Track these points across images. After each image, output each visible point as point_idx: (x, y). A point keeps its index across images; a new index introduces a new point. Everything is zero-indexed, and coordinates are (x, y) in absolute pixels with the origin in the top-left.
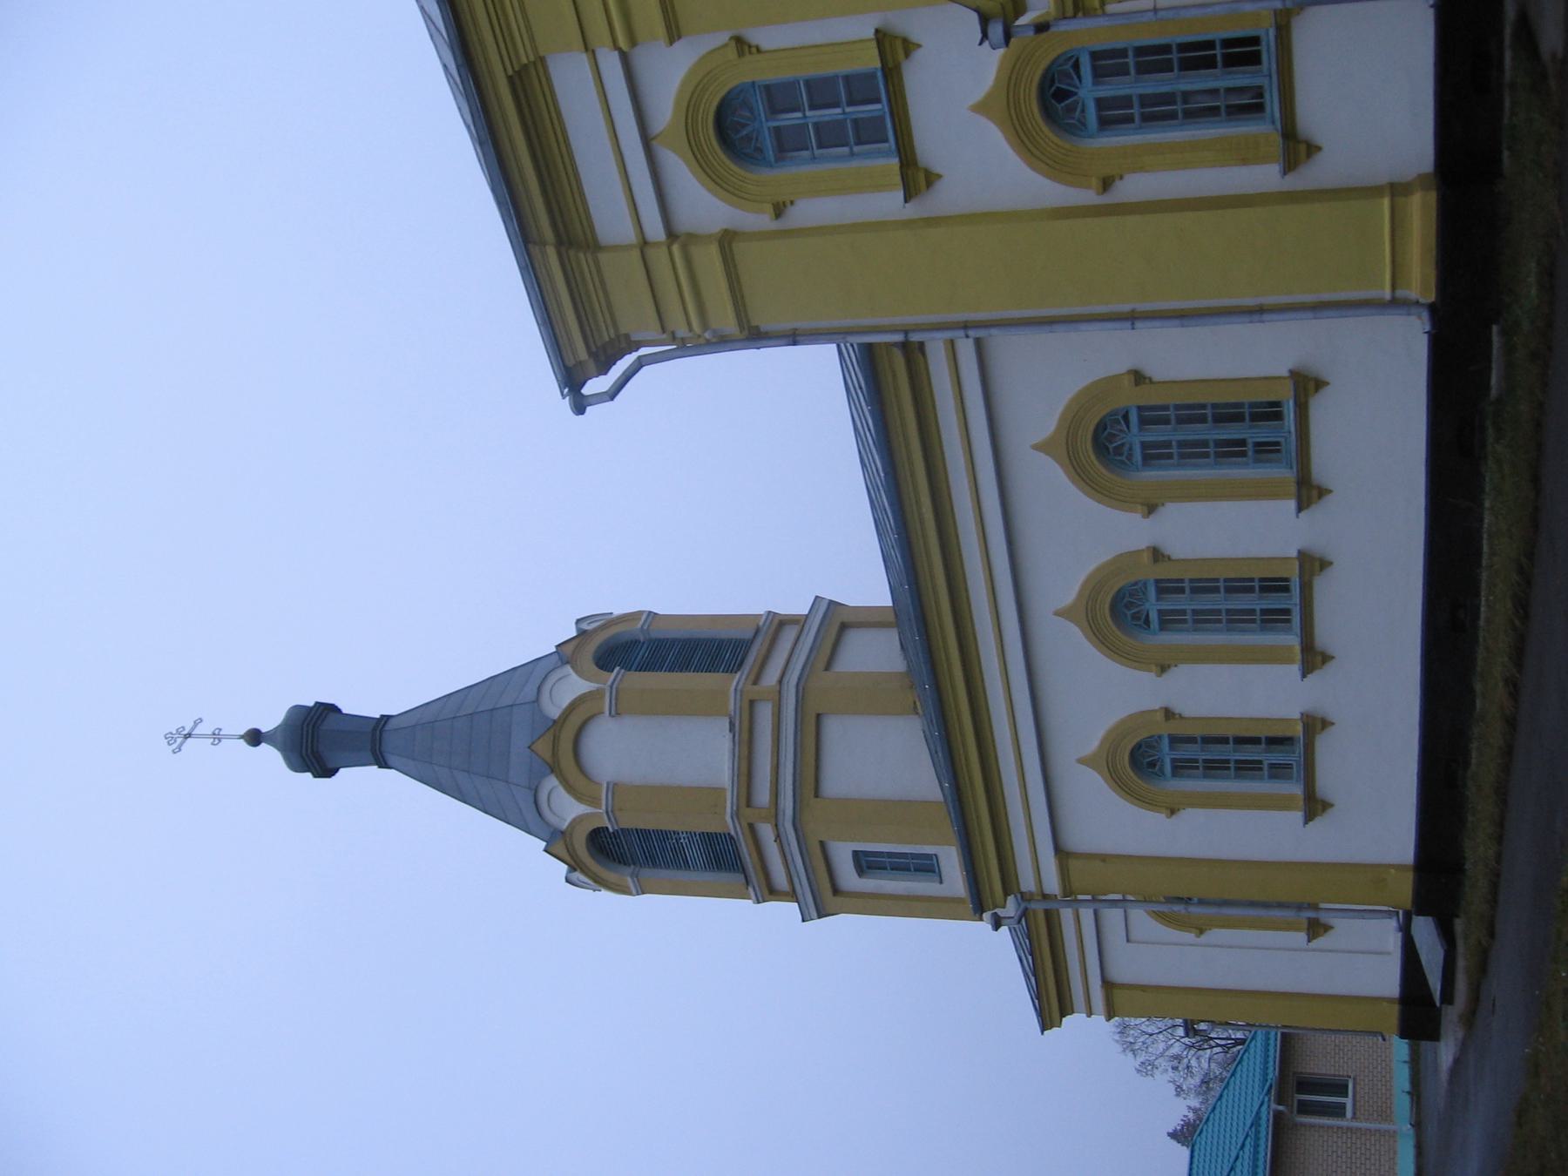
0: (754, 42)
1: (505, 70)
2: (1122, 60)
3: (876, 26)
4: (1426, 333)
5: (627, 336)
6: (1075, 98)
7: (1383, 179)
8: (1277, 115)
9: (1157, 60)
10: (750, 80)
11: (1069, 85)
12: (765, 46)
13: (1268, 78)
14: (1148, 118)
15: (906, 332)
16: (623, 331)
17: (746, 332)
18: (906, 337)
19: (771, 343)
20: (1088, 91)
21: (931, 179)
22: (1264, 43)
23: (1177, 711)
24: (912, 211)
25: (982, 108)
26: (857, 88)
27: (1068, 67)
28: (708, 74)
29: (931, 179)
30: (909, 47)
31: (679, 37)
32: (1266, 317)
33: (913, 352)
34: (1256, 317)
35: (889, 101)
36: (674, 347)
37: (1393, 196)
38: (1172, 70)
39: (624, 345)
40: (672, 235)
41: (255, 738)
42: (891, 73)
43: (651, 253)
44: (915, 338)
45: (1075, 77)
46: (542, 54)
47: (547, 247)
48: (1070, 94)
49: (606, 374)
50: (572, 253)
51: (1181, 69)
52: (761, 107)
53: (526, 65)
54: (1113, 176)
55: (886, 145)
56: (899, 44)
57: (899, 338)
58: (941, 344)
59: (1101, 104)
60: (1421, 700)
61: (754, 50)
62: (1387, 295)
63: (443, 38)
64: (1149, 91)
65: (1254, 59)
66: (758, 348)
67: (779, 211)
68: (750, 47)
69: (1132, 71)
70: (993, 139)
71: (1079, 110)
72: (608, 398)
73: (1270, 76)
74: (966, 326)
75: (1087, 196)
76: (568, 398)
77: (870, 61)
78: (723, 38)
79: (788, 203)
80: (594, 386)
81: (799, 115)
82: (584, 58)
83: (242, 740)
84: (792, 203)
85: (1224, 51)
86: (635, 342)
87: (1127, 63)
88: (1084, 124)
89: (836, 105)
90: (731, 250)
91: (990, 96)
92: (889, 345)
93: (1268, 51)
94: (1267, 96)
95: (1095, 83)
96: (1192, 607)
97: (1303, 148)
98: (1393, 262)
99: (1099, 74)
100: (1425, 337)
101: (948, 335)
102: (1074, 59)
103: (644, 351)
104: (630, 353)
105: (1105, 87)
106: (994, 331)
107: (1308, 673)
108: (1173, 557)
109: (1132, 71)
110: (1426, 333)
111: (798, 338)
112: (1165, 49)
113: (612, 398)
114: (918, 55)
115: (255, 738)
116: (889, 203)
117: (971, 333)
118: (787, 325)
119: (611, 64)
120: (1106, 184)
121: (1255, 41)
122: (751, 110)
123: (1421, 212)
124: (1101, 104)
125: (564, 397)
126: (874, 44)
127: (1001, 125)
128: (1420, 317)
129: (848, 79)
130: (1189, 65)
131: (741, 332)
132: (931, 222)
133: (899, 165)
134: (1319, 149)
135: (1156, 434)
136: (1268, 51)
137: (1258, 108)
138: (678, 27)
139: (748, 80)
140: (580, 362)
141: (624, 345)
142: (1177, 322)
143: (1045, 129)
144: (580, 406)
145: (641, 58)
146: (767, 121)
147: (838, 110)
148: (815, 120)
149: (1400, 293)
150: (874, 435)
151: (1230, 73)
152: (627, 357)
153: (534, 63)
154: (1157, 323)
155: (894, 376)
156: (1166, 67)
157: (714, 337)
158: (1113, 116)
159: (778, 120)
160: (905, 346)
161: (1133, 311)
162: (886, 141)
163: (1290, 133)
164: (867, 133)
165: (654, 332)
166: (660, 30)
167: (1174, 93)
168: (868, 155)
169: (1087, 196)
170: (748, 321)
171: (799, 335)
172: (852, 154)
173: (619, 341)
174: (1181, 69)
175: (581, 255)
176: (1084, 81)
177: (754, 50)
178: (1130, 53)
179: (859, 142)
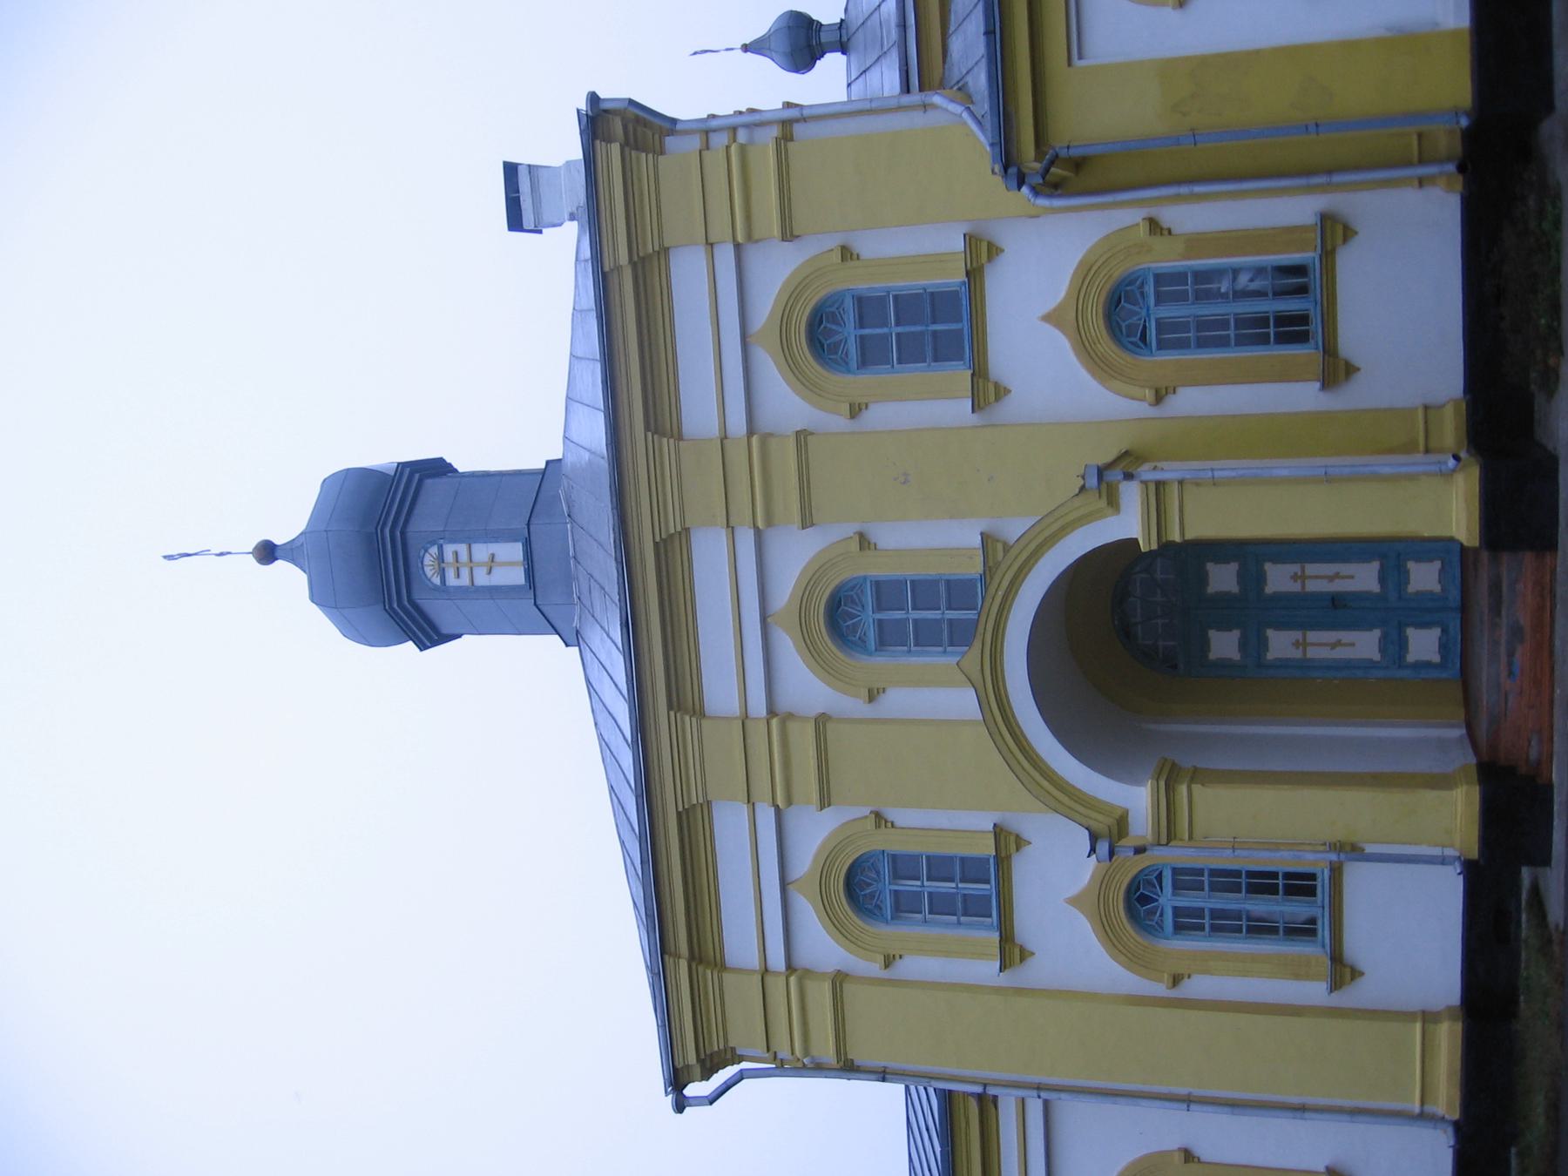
0: (890, 818)
1: (654, 537)
2: (1186, 335)
3: (964, 232)
4: (1459, 874)
5: (733, 1049)
6: (1156, 904)
7: (1415, 1005)
8: (1327, 941)
9: (1220, 335)
10: (882, 849)
11: (1152, 892)
12: (898, 823)
13: (1321, 909)
14: (1215, 929)
15: (985, 1086)
16: (731, 1044)
17: (842, 1063)
18: (985, 1089)
19: (862, 1076)
20: (1168, 900)
21: (1024, 955)
22: (1319, 880)
23: (1196, 1155)
24: (1004, 979)
25: (1075, 901)
26: (971, 869)
27: (1153, 877)
28: (848, 837)
29: (1024, 955)
30: (1020, 842)
31: (829, 805)
32: (1307, 1115)
33: (987, 1103)
34: (1298, 1114)
35: (997, 884)
36: (774, 1066)
37: (1424, 1022)
38: (1240, 892)
39: (729, 1056)
40: (790, 968)
41: (267, 553)
42: (1002, 862)
43: (769, 979)
44: (992, 1091)
45: (1158, 888)
46: (709, 799)
47: (680, 960)
48: (1151, 900)
49: (708, 1079)
50: (701, 969)
51: (1248, 891)
52: (886, 871)
53: (694, 805)
54: (1182, 975)
55: (989, 920)
56: (1012, 838)
57: (978, 1089)
58: (1013, 1098)
59: (1177, 911)
60: (1463, 293)
61: (889, 825)
62: (1417, 1109)
63: (624, 697)
64: (1219, 906)
65: (1310, 892)
66: (849, 1079)
67: (888, 962)
68: (886, 822)
69: (1207, 888)
70: (1083, 930)
71: (1158, 914)
72: (707, 1102)
73: (1323, 908)
74: (1039, 1088)
75: (1160, 989)
76: (671, 1096)
77: (987, 848)
78: (866, 811)
79: (897, 957)
80: (693, 1089)
81: (919, 883)
82: (744, 809)
83: (251, 555)
84: (901, 957)
85: (1286, 882)
86: (739, 1056)
87: (1203, 881)
88: (1162, 928)
89: (951, 880)
90: (841, 991)
91: (1087, 890)
92: (966, 1095)
93: (1323, 886)
94: (1319, 923)
95: (1174, 894)
96: (1212, 906)
97: (1347, 971)
98: (1423, 1044)
99: (1177, 886)
100: (1451, 1150)
101: (1021, 1093)
102: (1157, 872)
103: (745, 1065)
104: (732, 1065)
105: (1179, 898)
106: (1063, 1096)
107: (1335, 989)
108: (1202, 1159)
109: (1207, 888)
110: (1459, 874)
111: (887, 1076)
112: (1237, 874)
113: (711, 1103)
114: (1027, 849)
115: (267, 553)
116: (986, 970)
117: (1044, 1095)
118: (879, 1062)
119: (726, 256)
120: (1176, 980)
121: (1312, 877)
122: (878, 873)
123: (1448, 1038)
124: (1177, 911)
125: (667, 1094)
126: (992, 836)
127: (1089, 917)
128: (1445, 1132)
129: (963, 860)
130: (1254, 889)
131: (838, 1062)
132: (1020, 991)
133: (998, 939)
134: (1362, 974)
135: (1189, 900)
136: (1323, 886)
137: (1312, 933)
138: (829, 798)
139: (862, 573)
140: (688, 1065)
141: (729, 1056)
142: (1226, 1109)
143: (1128, 927)
144: (680, 1106)
145: (793, 817)
146: (890, 884)
147: (953, 885)
148: (930, 890)
149: (1429, 1108)
150: (940, 1168)
151: (1288, 901)
152: (729, 1068)
153: (680, 533)
154: (1210, 1108)
155: (967, 1123)
156: (1236, 888)
157: (812, 1063)
158: (1186, 922)
159: (897, 884)
160: (980, 1098)
161: (1189, 1094)
162: (990, 916)
163: (1337, 958)
164: (973, 908)
165: (760, 1050)
166: (815, 796)
167: (1241, 911)
168: (969, 925)
169: (1160, 989)
170: (846, 1054)
171: (888, 1073)
172: (959, 923)
173: (726, 1053)
174: (1248, 891)
175: (709, 972)
176: (1164, 891)
177: (889, 825)
178: (1206, 874)
179: (965, 914)
